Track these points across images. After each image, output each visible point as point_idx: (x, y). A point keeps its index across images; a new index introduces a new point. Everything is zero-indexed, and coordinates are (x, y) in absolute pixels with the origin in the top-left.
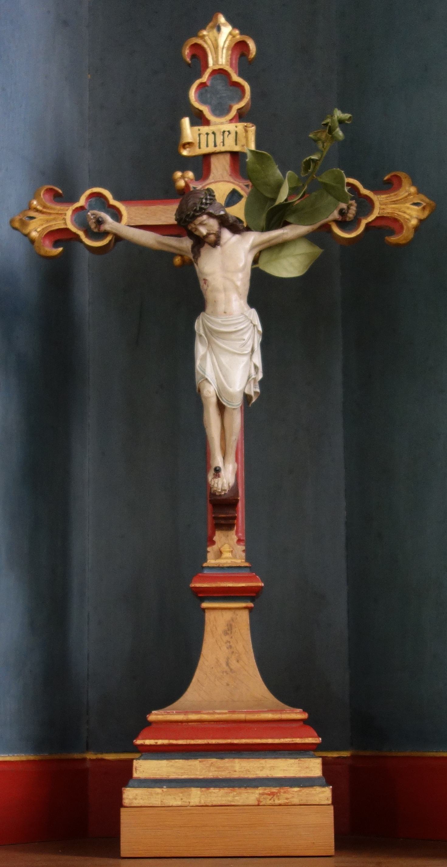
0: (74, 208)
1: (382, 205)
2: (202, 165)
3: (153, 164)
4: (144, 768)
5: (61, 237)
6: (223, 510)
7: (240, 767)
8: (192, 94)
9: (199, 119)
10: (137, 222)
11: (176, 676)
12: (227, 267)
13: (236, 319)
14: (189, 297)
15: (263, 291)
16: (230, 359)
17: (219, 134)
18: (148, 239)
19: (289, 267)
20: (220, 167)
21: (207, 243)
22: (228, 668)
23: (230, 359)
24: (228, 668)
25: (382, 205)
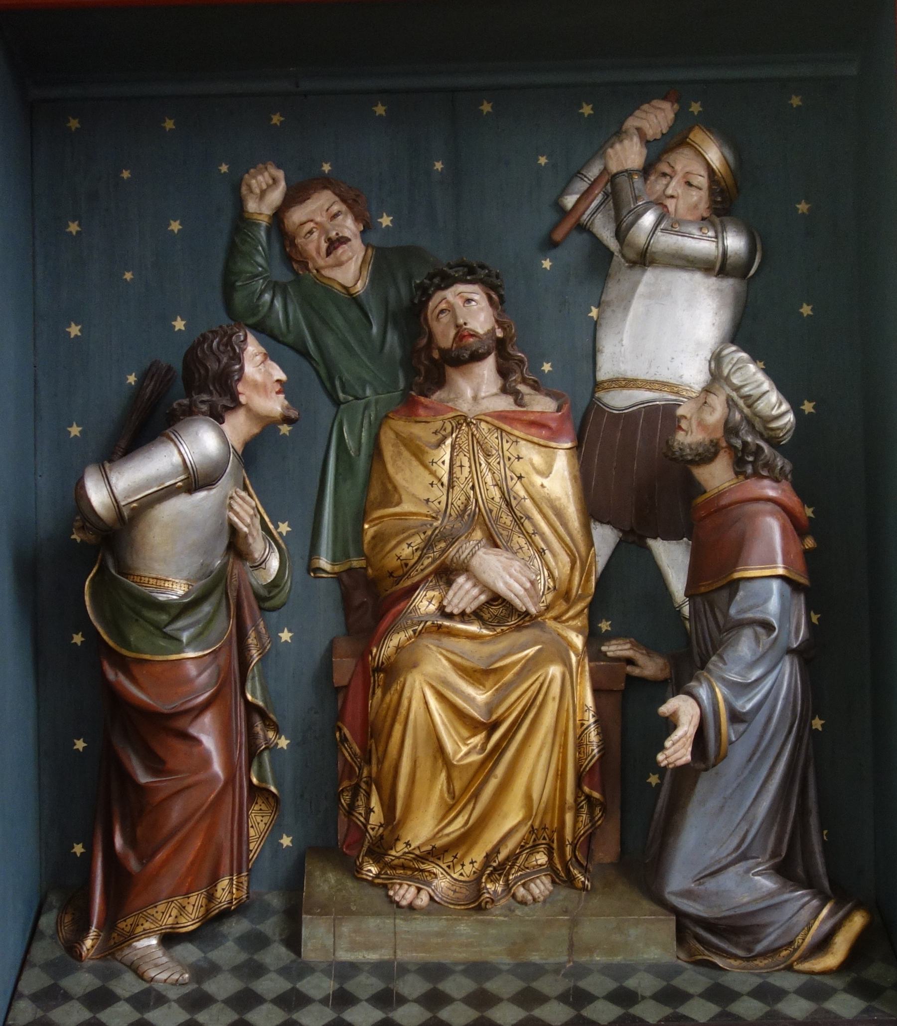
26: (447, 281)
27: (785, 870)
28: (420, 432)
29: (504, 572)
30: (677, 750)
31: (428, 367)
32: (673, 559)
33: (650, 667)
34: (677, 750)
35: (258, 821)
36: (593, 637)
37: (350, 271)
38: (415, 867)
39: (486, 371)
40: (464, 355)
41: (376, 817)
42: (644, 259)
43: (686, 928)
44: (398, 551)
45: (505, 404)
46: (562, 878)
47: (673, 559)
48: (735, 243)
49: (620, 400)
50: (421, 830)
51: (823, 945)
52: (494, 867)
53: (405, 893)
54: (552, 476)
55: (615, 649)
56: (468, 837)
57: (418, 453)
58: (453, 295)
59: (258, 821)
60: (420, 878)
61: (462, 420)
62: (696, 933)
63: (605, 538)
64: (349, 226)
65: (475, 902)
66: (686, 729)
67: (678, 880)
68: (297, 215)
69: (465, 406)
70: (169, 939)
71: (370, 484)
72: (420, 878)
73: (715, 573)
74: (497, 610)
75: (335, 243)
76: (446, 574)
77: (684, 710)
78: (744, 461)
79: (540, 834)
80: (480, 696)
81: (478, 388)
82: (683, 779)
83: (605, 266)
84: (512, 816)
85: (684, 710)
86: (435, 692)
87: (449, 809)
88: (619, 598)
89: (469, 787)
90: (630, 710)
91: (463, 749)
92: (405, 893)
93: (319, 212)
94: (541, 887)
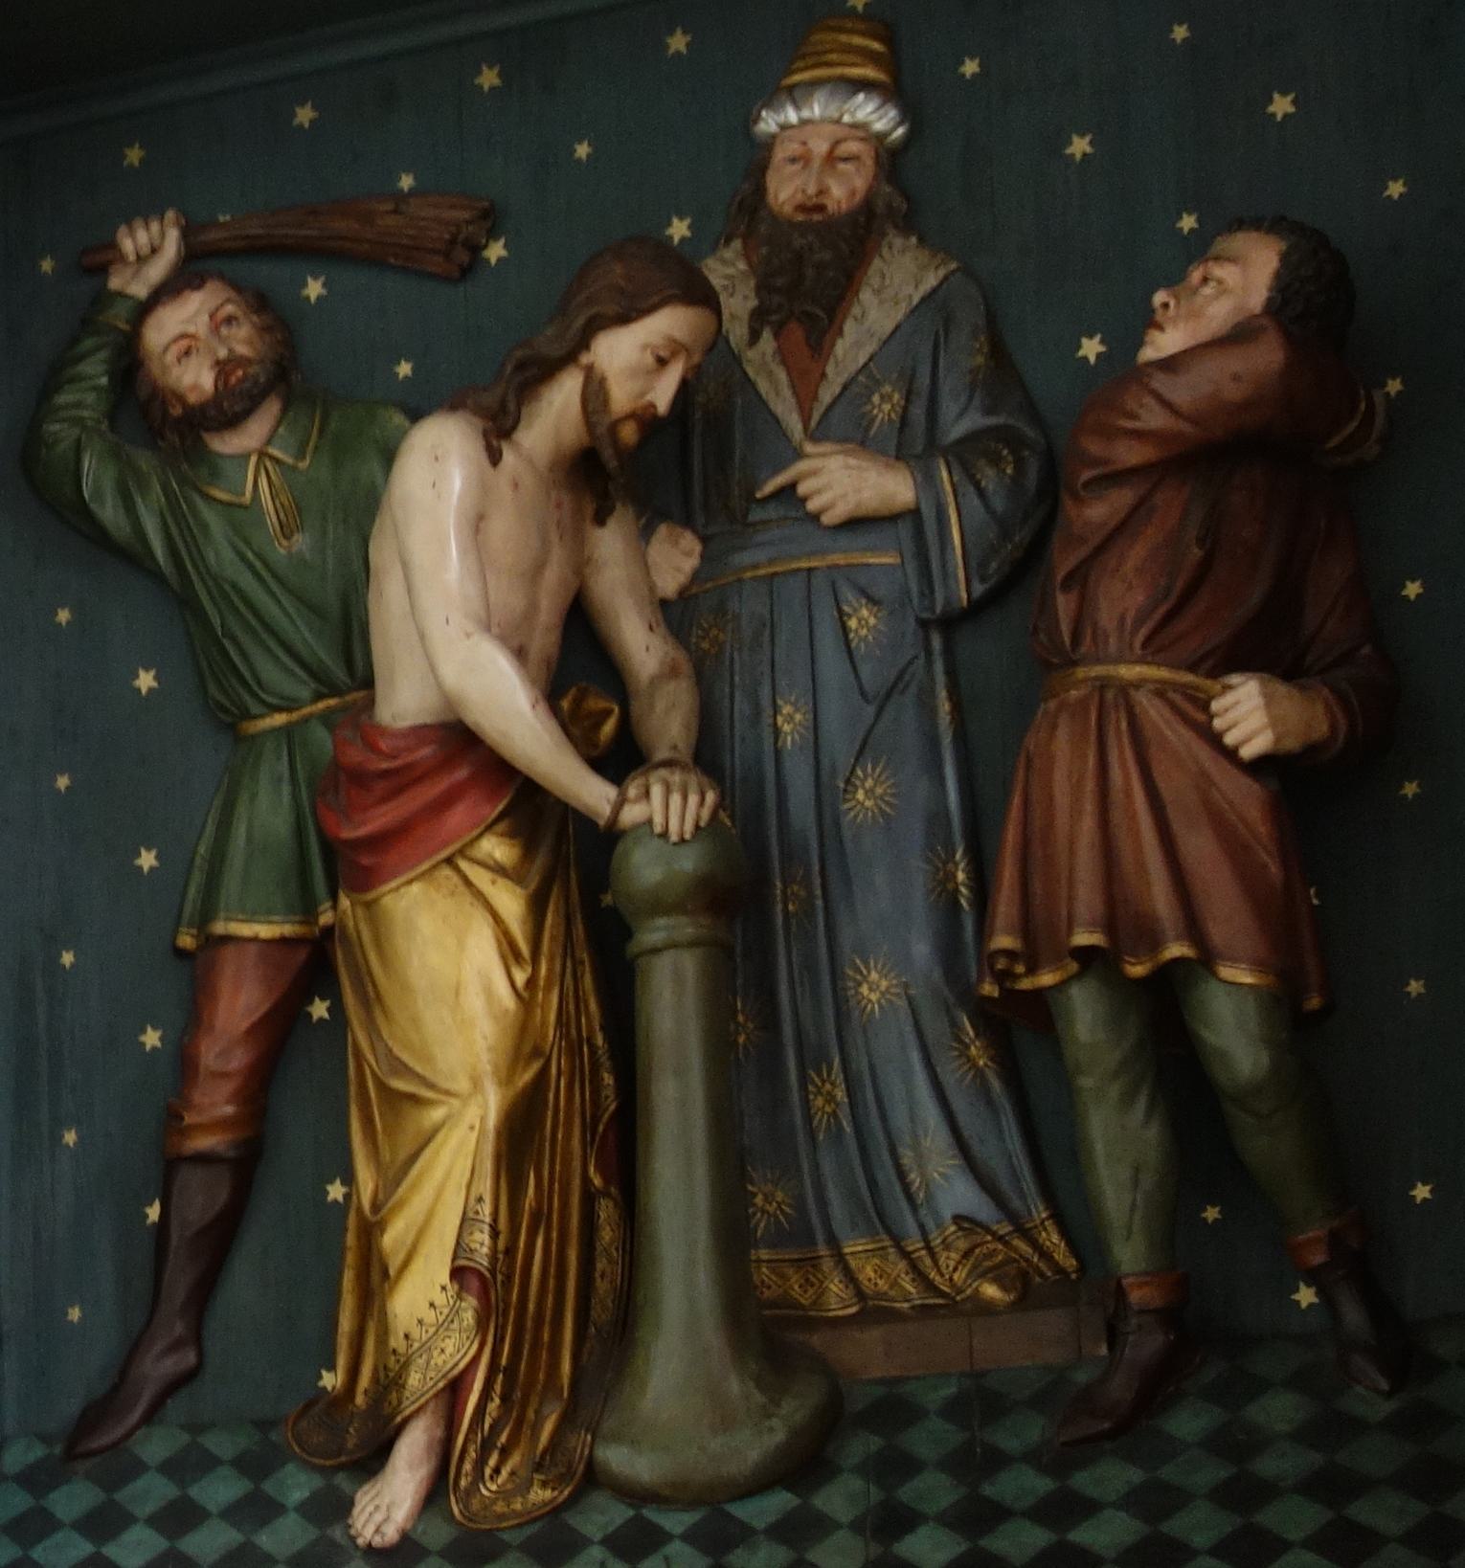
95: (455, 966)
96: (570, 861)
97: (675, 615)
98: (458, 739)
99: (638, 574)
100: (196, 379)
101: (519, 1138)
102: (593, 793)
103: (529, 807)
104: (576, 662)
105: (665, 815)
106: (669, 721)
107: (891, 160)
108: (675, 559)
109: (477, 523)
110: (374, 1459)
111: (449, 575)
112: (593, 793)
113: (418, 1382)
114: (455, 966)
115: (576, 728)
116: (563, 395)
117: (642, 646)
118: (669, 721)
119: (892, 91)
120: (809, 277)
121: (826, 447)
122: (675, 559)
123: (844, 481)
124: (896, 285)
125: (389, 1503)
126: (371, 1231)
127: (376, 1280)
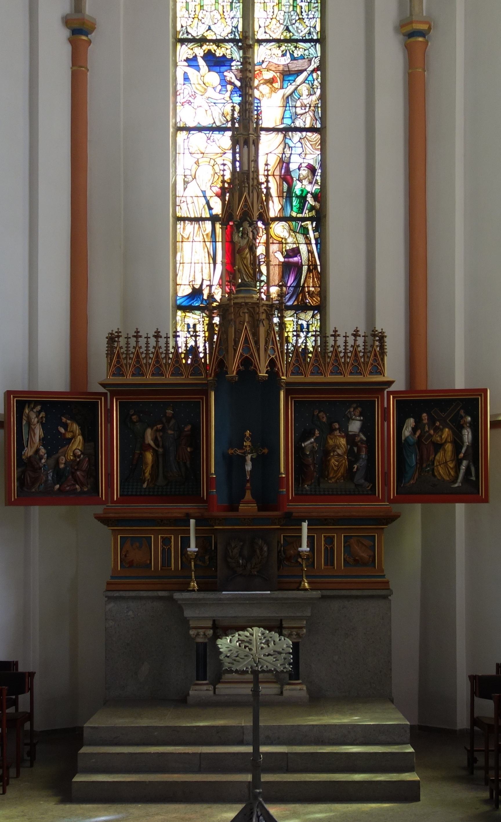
0: (389, 343)
1: (264, 451)
2: (246, 446)
3: (241, 446)
4: (241, 505)
5: (232, 453)
6: (248, 481)
7: (249, 505)
8: (456, 485)
9: (246, 442)
10: (239, 452)
11: (243, 497)
12: (249, 457)
13: (267, 688)
14: (245, 461)
15: (252, 459)
16: (249, 467)
17: (247, 443)
18: (241, 454)
19: (254, 457)
20: (248, 447)
21: (268, 130)
22: (248, 496)
23: (249, 467)
24: (248, 496)
25: (264, 451)
26: (334, 423)
27: (366, 480)
28: (332, 437)
29: (340, 452)
30: (355, 470)
31: (332, 430)
32: (356, 449)
33: (353, 459)
34: (355, 470)
35: (315, 474)
36: (347, 456)
37: (324, 420)
38: (330, 479)
39: (338, 431)
40: (335, 430)
41: (327, 474)
42: (353, 420)
43: (356, 485)
44: (180, 294)
45: (339, 434)
46: (344, 480)
47: (356, 449)
48: (362, 418)
49: (350, 433)
50: (331, 475)
51: (368, 487)
52: (338, 479)
53: (330, 481)
54: (343, 441)
55: (350, 458)
56: (336, 476)
57: (332, 439)
58: (335, 424)
59: (315, 474)
60: (331, 480)
61: (335, 436)
62: (356, 485)
63: (349, 446)
64: (324, 416)
65: (336, 482)
66: (356, 468)
67: (355, 481)
68: (319, 414)
69: (336, 434)
70: (308, 485)
71: (326, 440)
72: (331, 480)
73: (359, 450)
74: (338, 455)
75: (323, 417)
76: (334, 451)
77: (356, 466)
78: (361, 443)
79: (342, 476)
80: (337, 463)
81: (337, 433)
82: (355, 472)
83: (349, 419)
84: (340, 474)
85: (356, 466)
86: (333, 462)
87: (333, 474)
88: (350, 452)
89: (336, 472)
90: (351, 464)
91: (335, 468)
92: (330, 481)
93: (321, 414)
94: (342, 481)
95: (149, 456)
96: (156, 454)
97: (161, 437)
98: (149, 445)
99: (159, 435)
100: (135, 420)
101: (152, 466)
102: (157, 449)
103: (153, 449)
104: (155, 440)
105: (161, 450)
106: (161, 444)
107: (173, 414)
108: (161, 434)
109: (151, 434)
110: (144, 483)
111: (149, 436)
112: (157, 449)
113: (147, 479)
114: (149, 456)
115: (155, 443)
116: (155, 427)
117: (159, 439)
118: (161, 444)
119: (173, 411)
120: (169, 420)
121: (226, 303)
122: (161, 434)
123: (170, 432)
124: (173, 422)
125: (145, 485)
126: (144, 471)
127: (144, 473)
